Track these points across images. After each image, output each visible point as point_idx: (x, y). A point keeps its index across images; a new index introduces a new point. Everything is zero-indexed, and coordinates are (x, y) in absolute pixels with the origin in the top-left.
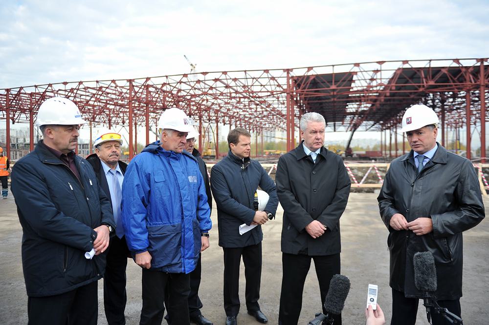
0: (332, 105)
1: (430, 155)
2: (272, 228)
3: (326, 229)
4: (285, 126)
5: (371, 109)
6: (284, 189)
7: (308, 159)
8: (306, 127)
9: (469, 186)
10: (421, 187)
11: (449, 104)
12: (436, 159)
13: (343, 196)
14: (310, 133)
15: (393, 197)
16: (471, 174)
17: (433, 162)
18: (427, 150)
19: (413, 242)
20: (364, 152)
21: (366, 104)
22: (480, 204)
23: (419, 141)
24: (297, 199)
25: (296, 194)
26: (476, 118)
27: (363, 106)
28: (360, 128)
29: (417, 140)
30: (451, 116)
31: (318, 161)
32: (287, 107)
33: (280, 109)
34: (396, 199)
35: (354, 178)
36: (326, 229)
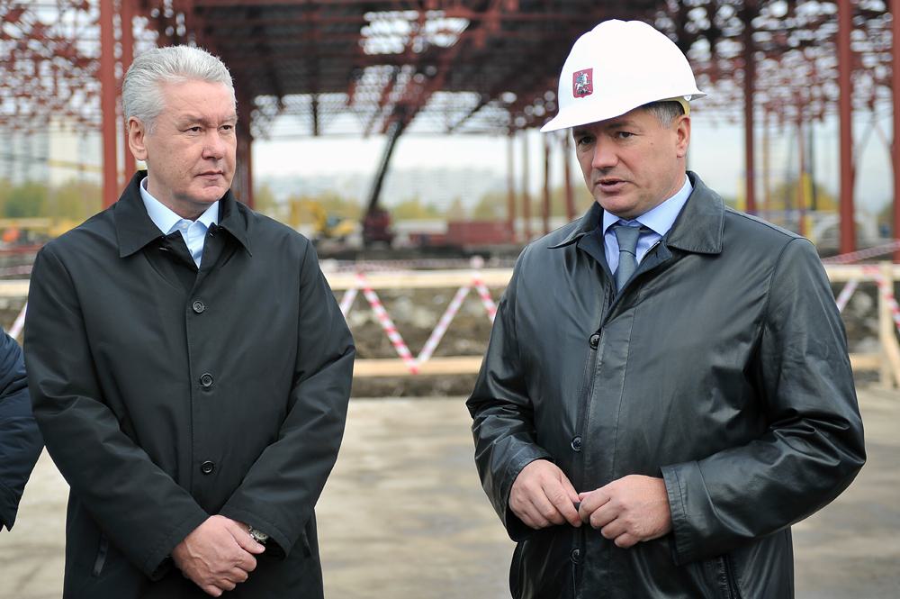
0: (302, 17)
1: (660, 220)
2: (27, 579)
3: (261, 549)
4: (92, 109)
5: (465, 40)
6: (66, 390)
7: (167, 249)
8: (160, 103)
9: (805, 340)
10: (625, 350)
11: (774, 25)
12: (680, 239)
13: (324, 401)
14: (183, 130)
15: (526, 394)
16: (811, 294)
17: (671, 248)
18: (652, 203)
19: (600, 573)
20: (437, 227)
21: (447, 17)
22: (846, 412)
23: (621, 166)
24: (132, 431)
25: (125, 408)
26: (877, 82)
27: (431, 27)
28: (421, 123)
29: (612, 161)
30: (778, 77)
31: (213, 257)
32: (103, 22)
33: (69, 32)
34: (537, 402)
35: (395, 337)
36: (261, 549)
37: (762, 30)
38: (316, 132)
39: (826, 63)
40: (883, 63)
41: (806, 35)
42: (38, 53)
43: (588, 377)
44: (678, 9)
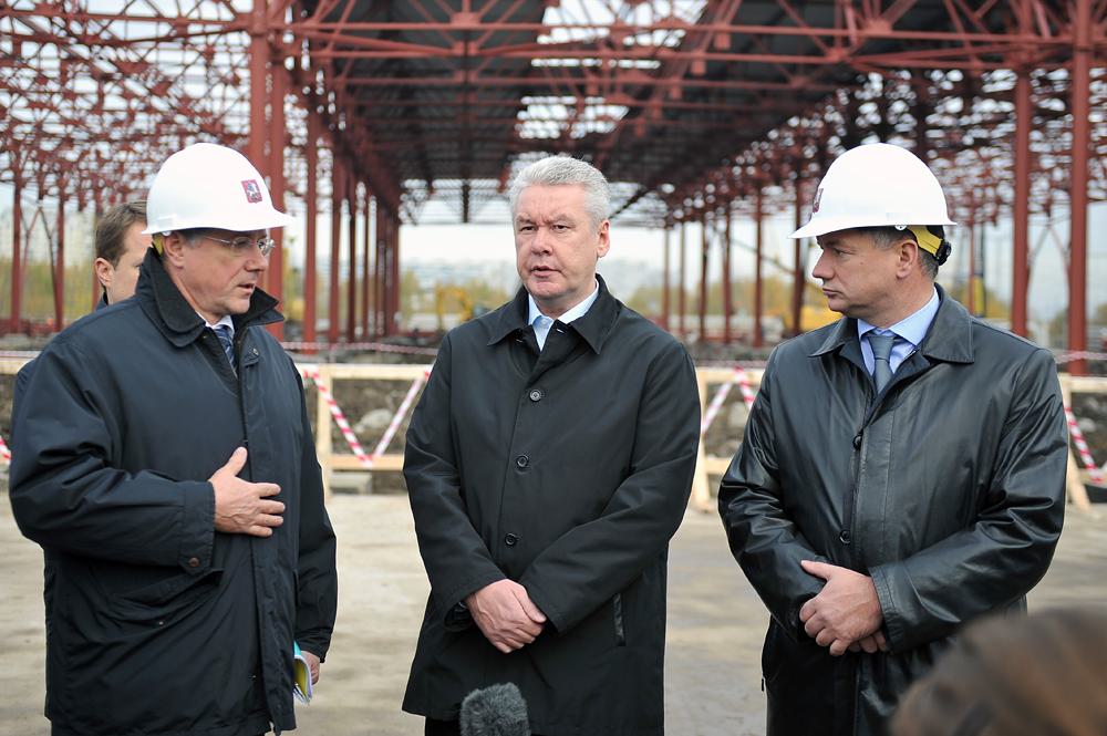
5: (624, 128)
11: (948, 121)
12: (935, 348)
17: (927, 357)
26: (1054, 185)
27: (590, 113)
32: (256, 101)
33: (216, 107)
37: (935, 127)
38: (466, 219)
39: (1001, 164)
40: (1061, 166)
41: (983, 134)
42: (184, 127)
43: (853, 474)
44: (847, 102)
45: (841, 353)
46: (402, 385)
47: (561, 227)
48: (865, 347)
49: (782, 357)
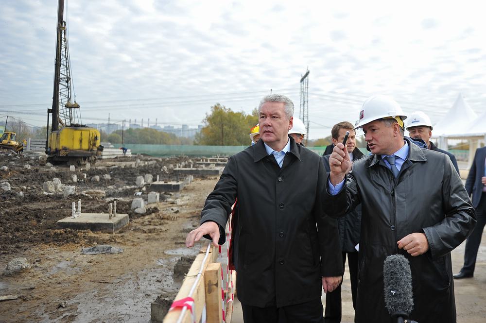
45: (379, 164)
46: (217, 172)
47: (274, 117)
48: (386, 161)
49: (354, 167)
